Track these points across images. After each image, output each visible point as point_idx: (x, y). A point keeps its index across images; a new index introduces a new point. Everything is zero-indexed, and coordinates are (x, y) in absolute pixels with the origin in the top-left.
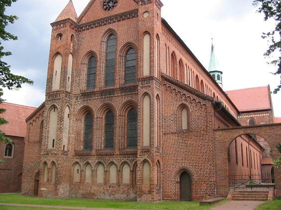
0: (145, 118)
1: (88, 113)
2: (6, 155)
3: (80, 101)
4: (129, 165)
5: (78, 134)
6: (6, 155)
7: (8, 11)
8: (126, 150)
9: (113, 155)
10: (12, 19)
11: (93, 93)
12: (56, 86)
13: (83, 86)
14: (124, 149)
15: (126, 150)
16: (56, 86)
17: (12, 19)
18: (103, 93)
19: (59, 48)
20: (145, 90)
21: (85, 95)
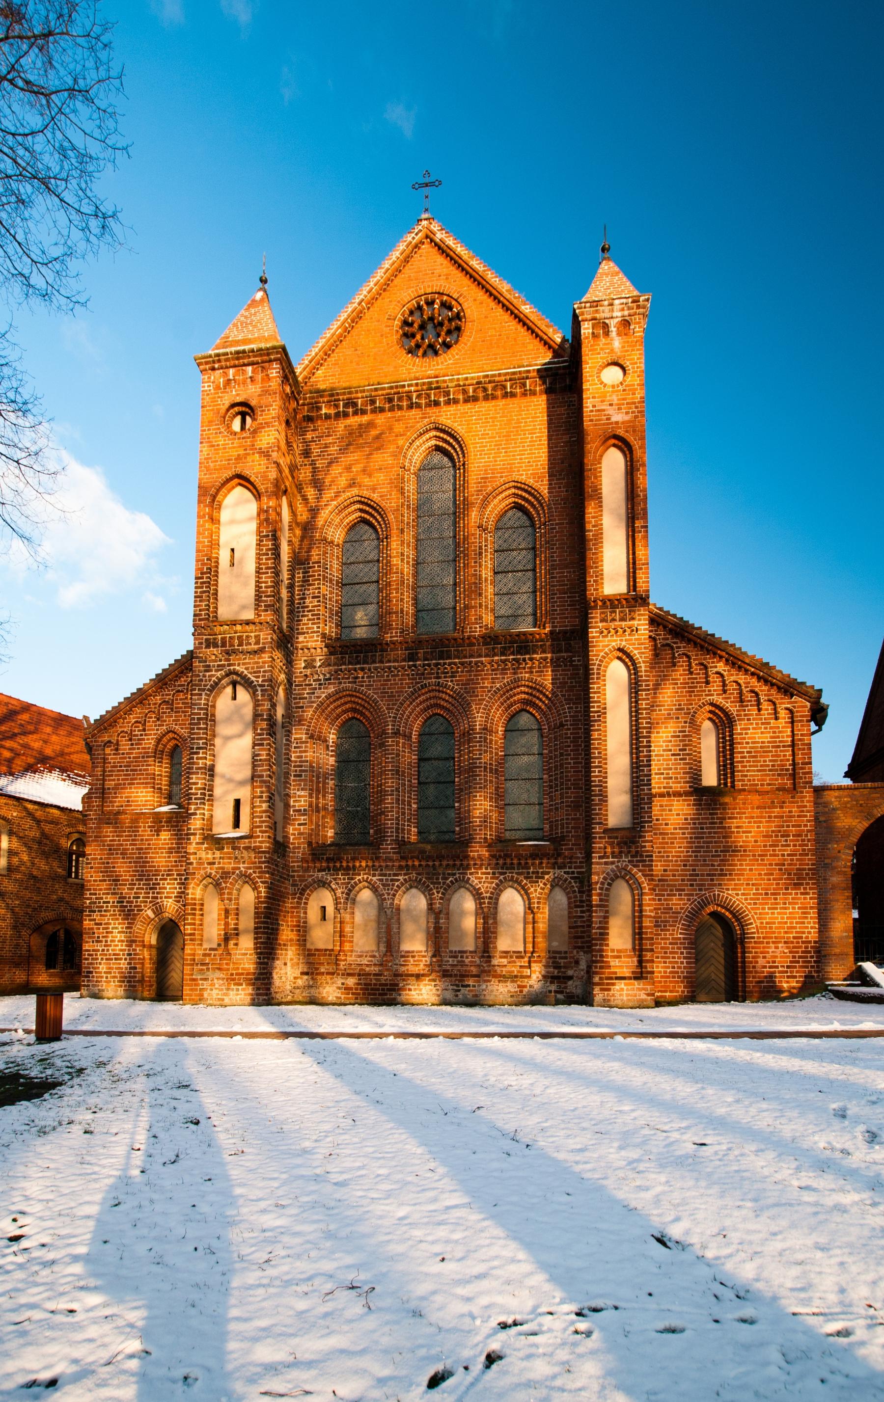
20: (615, 642)
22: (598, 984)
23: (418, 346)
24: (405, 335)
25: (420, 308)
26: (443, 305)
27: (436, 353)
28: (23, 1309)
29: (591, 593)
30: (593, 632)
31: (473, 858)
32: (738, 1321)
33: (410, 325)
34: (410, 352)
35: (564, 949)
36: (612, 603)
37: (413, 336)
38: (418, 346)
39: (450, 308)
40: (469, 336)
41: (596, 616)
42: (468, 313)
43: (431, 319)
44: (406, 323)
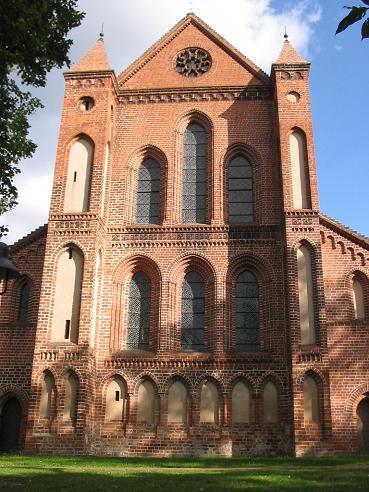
5: (117, 313)
9: (212, 362)
16: (74, 203)
19: (84, 125)
20: (301, 236)
22: (298, 444)
23: (186, 71)
24: (178, 65)
25: (186, 53)
26: (199, 52)
27: (196, 75)
28: (91, 148)
29: (287, 209)
30: (288, 230)
31: (217, 362)
32: (338, 31)
33: (182, 60)
34: (181, 73)
35: (274, 421)
36: (297, 215)
37: (183, 66)
38: (186, 71)
39: (203, 54)
40: (214, 70)
41: (289, 222)
42: (213, 58)
43: (193, 58)
44: (178, 59)
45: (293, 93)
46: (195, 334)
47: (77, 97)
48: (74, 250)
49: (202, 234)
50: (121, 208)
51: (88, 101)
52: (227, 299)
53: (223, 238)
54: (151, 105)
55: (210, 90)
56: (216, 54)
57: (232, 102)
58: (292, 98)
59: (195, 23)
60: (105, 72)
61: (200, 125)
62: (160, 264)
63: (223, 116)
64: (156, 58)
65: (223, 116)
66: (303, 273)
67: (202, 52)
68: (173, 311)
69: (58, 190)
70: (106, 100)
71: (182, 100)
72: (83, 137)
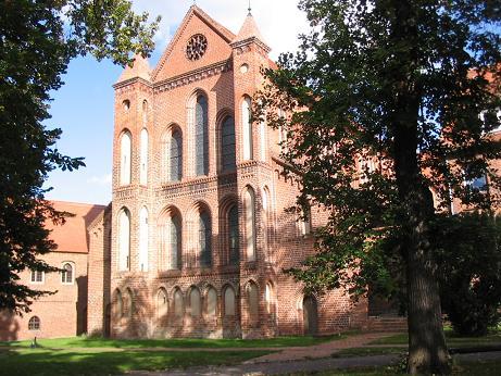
0: (215, 166)
1: (175, 215)
2: (33, 280)
3: (162, 198)
4: (233, 289)
5: (162, 246)
6: (33, 280)
7: (48, 125)
8: (230, 267)
10: (57, 133)
11: (180, 186)
12: (125, 180)
13: (166, 176)
14: (226, 265)
15: (230, 267)
16: (125, 180)
17: (57, 133)
18: (193, 185)
19: (127, 121)
20: (247, 182)
21: (169, 189)
30: (239, 178)
36: (245, 166)
45: (244, 64)
46: (206, 256)
47: (122, 101)
48: (126, 210)
49: (203, 183)
50: (159, 173)
51: (127, 102)
52: (338, 205)
53: (214, 185)
54: (173, 91)
55: (205, 69)
56: (211, 37)
57: (218, 76)
58: (244, 69)
59: (196, 13)
60: (249, 40)
61: (202, 98)
62: (181, 210)
63: (213, 90)
64: (170, 58)
65: (213, 90)
66: (250, 214)
67: (202, 37)
68: (193, 243)
69: (116, 171)
70: (139, 96)
71: (209, 76)
72: (126, 130)
